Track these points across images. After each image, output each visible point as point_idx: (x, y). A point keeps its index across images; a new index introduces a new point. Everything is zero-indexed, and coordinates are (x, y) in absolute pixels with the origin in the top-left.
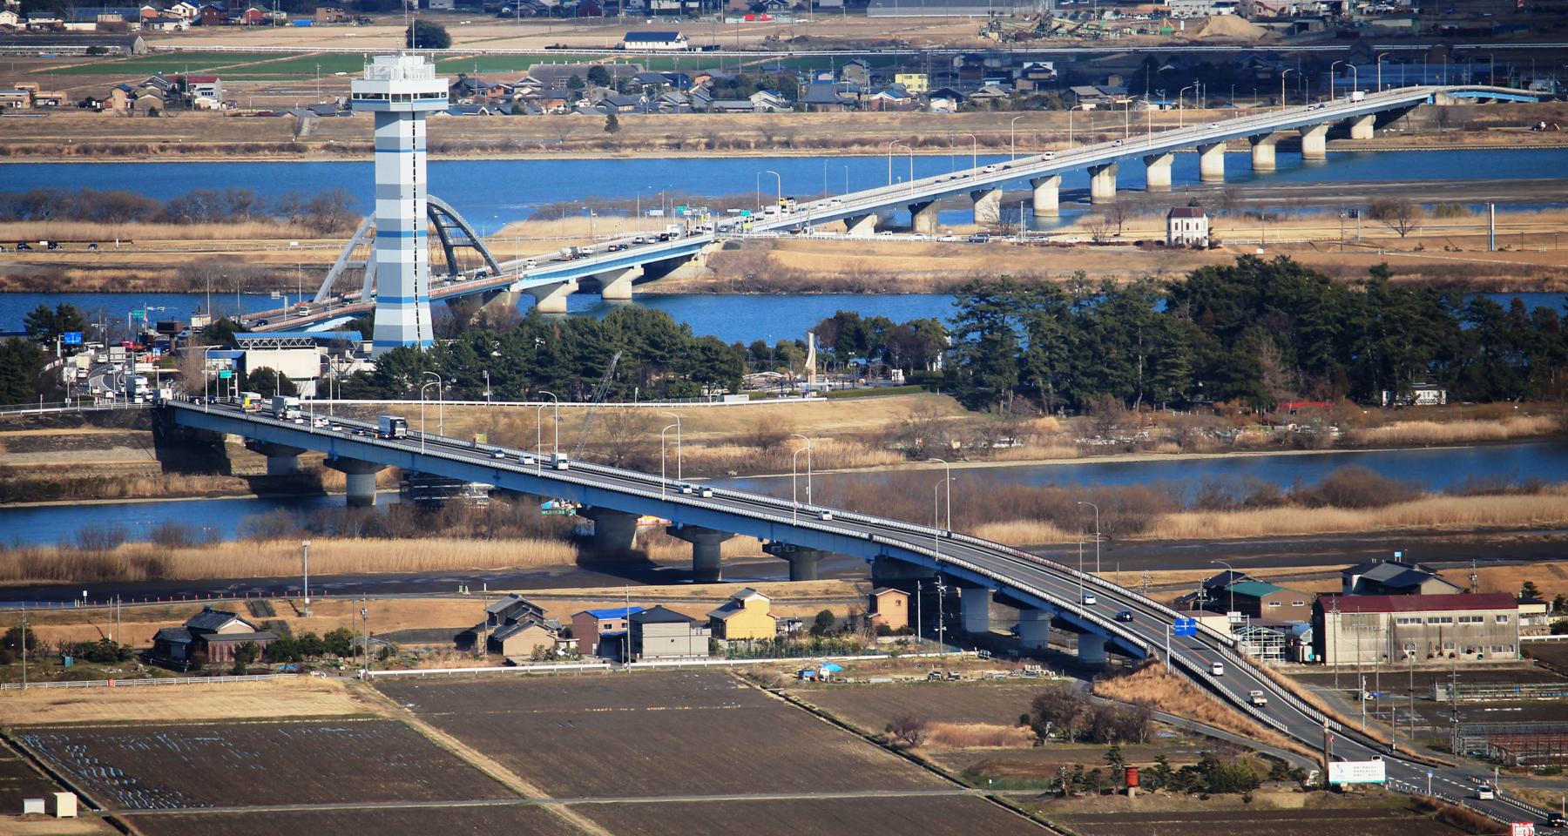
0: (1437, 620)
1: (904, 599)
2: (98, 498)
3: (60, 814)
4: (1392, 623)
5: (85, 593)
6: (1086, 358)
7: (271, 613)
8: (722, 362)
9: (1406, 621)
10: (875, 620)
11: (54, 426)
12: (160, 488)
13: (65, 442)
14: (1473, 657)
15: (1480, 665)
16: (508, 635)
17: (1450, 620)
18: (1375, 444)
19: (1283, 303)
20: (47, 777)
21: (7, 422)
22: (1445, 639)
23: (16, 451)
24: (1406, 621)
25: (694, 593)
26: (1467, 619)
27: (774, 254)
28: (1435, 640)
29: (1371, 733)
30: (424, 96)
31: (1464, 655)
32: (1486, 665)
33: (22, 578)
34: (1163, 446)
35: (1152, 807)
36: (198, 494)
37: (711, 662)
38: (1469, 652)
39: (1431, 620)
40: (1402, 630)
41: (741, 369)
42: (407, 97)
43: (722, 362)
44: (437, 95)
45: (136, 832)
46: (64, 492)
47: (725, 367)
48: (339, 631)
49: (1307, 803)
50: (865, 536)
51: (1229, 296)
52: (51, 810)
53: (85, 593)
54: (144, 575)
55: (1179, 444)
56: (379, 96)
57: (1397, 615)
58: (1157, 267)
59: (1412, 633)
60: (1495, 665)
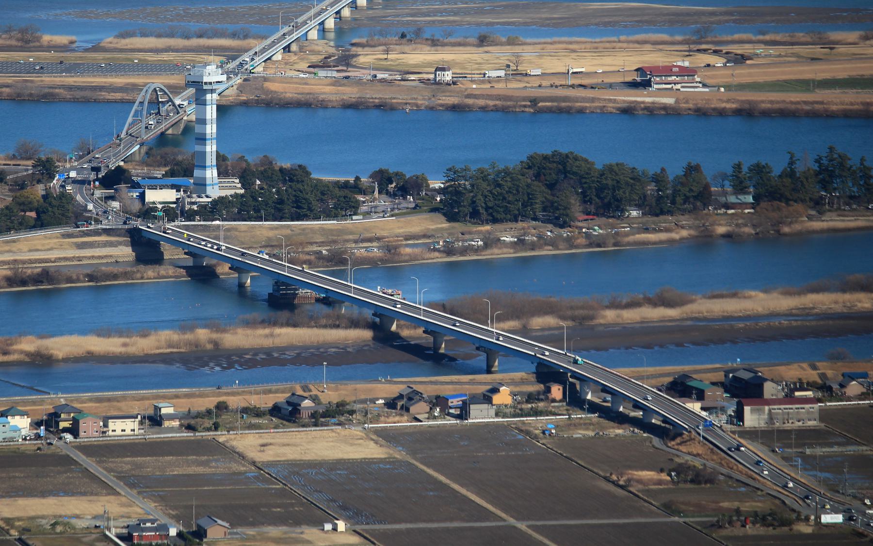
0: (787, 409)
1: (561, 388)
2: (133, 279)
3: (339, 530)
4: (770, 410)
5: (237, 382)
6: (499, 200)
7: (310, 391)
8: (352, 202)
9: (775, 409)
10: (550, 396)
11: (91, 236)
12: (156, 274)
13: (99, 244)
14: (800, 424)
15: (803, 426)
16: (412, 405)
17: (792, 409)
18: (629, 244)
19: (575, 174)
20: (306, 501)
21: (72, 234)
22: (790, 416)
23: (80, 249)
24: (775, 409)
25: (471, 380)
26: (798, 408)
27: (267, 85)
28: (786, 417)
29: (802, 480)
30: (217, 82)
31: (797, 423)
32: (806, 426)
33: (166, 348)
34: (546, 248)
35: (755, 533)
36: (171, 277)
37: (496, 420)
38: (799, 421)
39: (785, 409)
40: (774, 413)
41: (359, 205)
42: (210, 83)
43: (352, 202)
44: (221, 82)
45: (379, 544)
46: (119, 277)
47: (353, 204)
48: (342, 401)
49: (813, 531)
50: (533, 354)
51: (550, 169)
52: (335, 529)
53: (237, 382)
54: (212, 346)
55: (553, 247)
56: (199, 82)
57: (771, 407)
58: (432, 94)
59: (777, 414)
60: (809, 426)
